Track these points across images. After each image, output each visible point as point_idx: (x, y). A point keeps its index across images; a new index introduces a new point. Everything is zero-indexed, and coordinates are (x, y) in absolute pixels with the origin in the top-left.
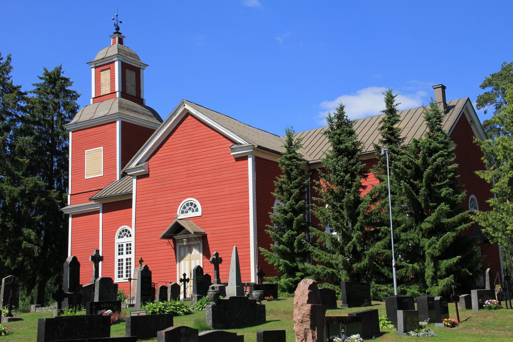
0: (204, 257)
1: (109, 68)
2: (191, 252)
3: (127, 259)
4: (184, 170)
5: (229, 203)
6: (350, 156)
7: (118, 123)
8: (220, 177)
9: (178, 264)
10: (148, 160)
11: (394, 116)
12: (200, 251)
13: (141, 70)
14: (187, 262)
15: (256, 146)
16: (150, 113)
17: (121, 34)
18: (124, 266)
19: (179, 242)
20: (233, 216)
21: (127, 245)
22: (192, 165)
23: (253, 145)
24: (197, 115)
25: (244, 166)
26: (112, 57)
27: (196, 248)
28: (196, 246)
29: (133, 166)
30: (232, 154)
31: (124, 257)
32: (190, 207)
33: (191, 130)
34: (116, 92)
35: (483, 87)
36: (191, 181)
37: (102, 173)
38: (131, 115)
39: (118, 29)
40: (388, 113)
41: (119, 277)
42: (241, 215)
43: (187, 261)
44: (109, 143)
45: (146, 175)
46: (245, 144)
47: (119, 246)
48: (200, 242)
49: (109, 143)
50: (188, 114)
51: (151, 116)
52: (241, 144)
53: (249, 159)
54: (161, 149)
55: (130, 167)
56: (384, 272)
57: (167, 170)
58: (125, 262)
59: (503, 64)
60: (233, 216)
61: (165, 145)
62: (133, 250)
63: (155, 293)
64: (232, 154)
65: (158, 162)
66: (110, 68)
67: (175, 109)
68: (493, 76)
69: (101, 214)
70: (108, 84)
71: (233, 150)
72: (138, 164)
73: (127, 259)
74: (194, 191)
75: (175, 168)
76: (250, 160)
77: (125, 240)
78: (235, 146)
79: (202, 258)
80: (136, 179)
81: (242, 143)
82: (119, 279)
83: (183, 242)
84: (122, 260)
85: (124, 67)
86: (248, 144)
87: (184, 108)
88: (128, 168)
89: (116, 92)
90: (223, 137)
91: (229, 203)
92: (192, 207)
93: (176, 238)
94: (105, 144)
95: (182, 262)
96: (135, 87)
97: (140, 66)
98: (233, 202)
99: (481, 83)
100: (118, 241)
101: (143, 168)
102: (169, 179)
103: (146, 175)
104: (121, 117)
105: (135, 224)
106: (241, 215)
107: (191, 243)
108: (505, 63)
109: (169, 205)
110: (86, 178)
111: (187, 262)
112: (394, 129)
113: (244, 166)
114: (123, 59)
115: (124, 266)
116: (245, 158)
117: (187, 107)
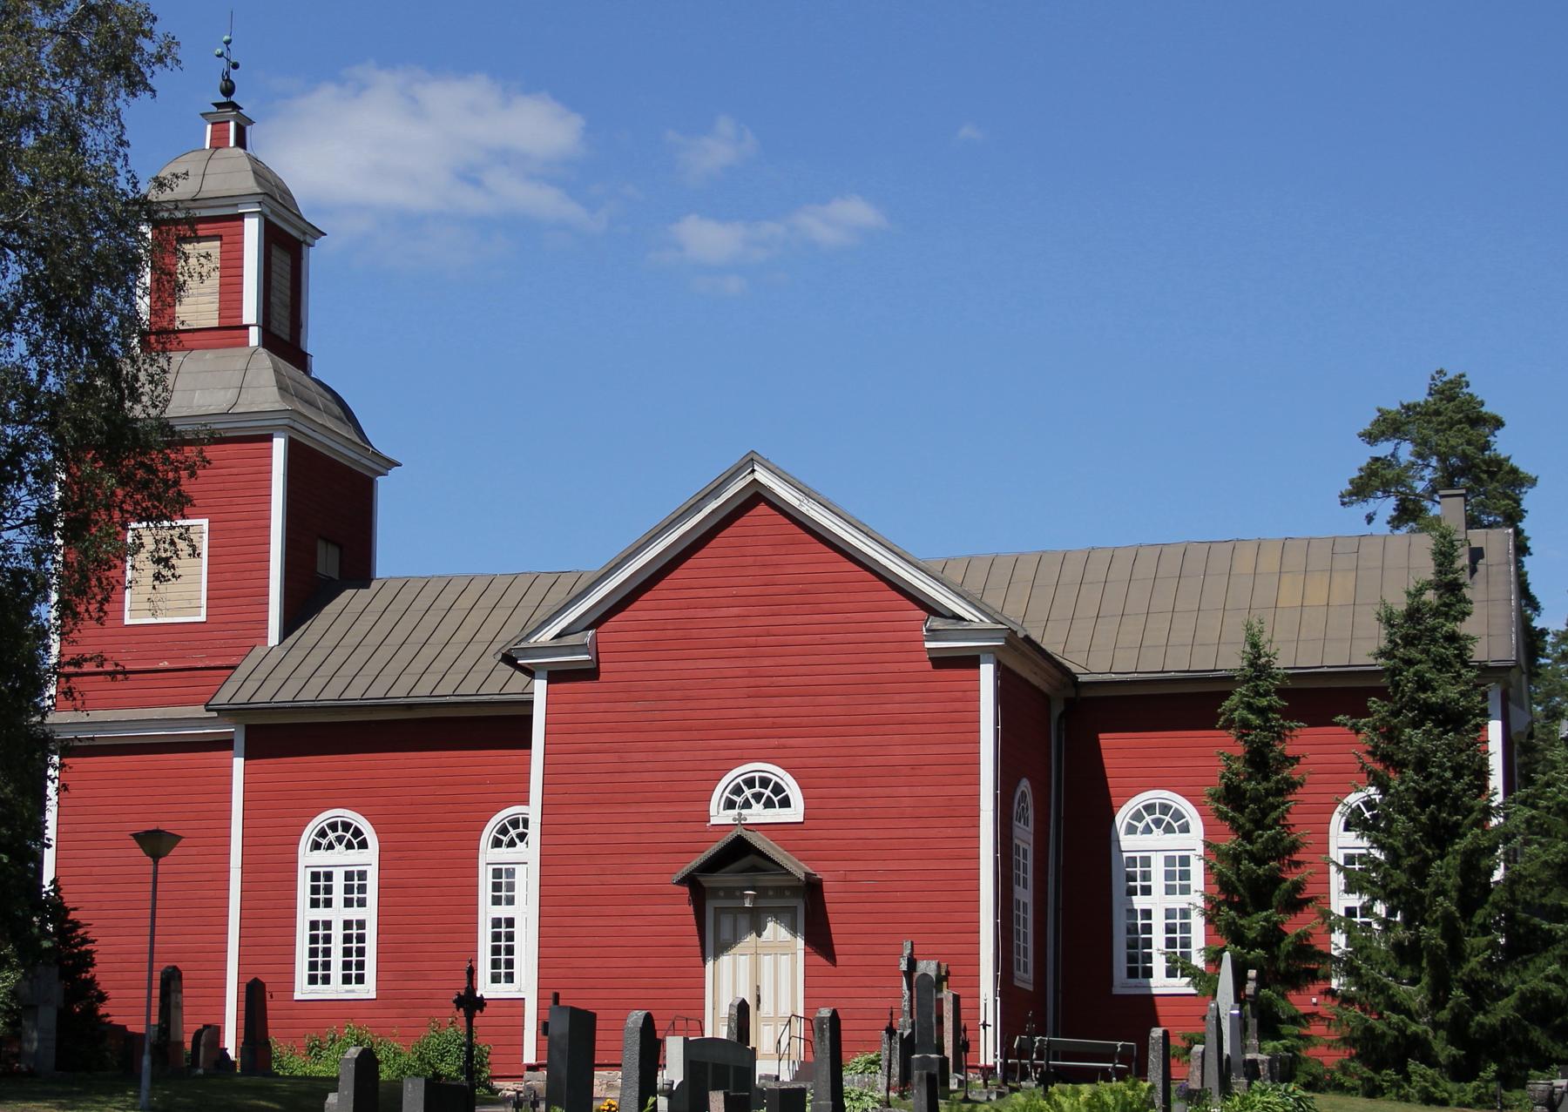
0: (809, 950)
1: (219, 237)
2: (759, 931)
3: (347, 924)
4: (739, 672)
5: (905, 791)
6: (1449, 725)
7: (279, 446)
8: (875, 709)
9: (710, 964)
10: (596, 624)
11: (1459, 601)
12: (793, 930)
13: (304, 247)
14: (744, 962)
15: (1021, 635)
16: (337, 410)
17: (240, 111)
18: (337, 946)
19: (716, 897)
20: (919, 833)
21: (349, 876)
22: (767, 662)
23: (1010, 629)
24: (804, 509)
25: (967, 686)
26: (235, 201)
27: (778, 919)
28: (778, 914)
29: (542, 639)
30: (928, 645)
31: (338, 914)
32: (757, 789)
33: (769, 550)
34: (247, 327)
35: (1371, 437)
36: (764, 711)
37: (204, 611)
38: (317, 420)
39: (228, 90)
40: (1442, 591)
41: (313, 980)
42: (950, 832)
43: (783, 957)
44: (234, 509)
45: (588, 673)
46: (977, 620)
47: (315, 876)
48: (800, 905)
49: (234, 509)
50: (757, 496)
51: (337, 418)
52: (961, 619)
53: (981, 666)
54: (647, 596)
55: (532, 640)
56: (1536, 1039)
57: (670, 665)
58: (337, 933)
59: (1436, 376)
60: (919, 833)
61: (662, 584)
62: (372, 895)
63: (660, 1051)
64: (928, 645)
65: (638, 635)
66: (221, 236)
67: (721, 479)
68: (1407, 408)
69: (238, 763)
70: (209, 290)
71: (934, 634)
72: (558, 636)
73: (347, 924)
74: (775, 742)
75: (700, 664)
76: (987, 672)
77: (340, 859)
78: (937, 623)
79: (801, 954)
80: (546, 681)
81: (967, 616)
82: (313, 987)
83: (743, 897)
84: (328, 925)
85: (273, 237)
86: (988, 624)
87: (750, 478)
88: (523, 645)
89: (247, 327)
90: (888, 588)
91: (905, 791)
92: (767, 792)
93: (705, 885)
94: (216, 510)
95: (725, 960)
96: (289, 311)
97: (304, 233)
98: (919, 791)
99: (1366, 421)
100: (308, 859)
101: (585, 650)
102: (678, 694)
103: (588, 673)
104: (292, 424)
105: (541, 824)
106: (950, 832)
107: (763, 903)
108: (1440, 372)
109: (676, 776)
110: (128, 621)
111: (744, 962)
112: (1461, 639)
113: (967, 686)
114: (272, 212)
115: (337, 946)
116: (970, 661)
117: (762, 476)
